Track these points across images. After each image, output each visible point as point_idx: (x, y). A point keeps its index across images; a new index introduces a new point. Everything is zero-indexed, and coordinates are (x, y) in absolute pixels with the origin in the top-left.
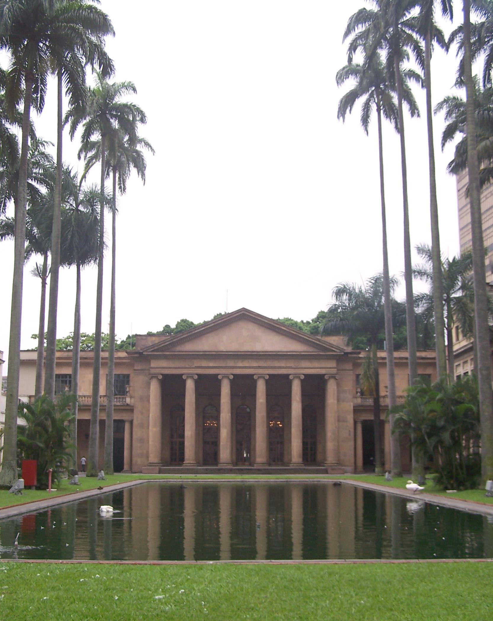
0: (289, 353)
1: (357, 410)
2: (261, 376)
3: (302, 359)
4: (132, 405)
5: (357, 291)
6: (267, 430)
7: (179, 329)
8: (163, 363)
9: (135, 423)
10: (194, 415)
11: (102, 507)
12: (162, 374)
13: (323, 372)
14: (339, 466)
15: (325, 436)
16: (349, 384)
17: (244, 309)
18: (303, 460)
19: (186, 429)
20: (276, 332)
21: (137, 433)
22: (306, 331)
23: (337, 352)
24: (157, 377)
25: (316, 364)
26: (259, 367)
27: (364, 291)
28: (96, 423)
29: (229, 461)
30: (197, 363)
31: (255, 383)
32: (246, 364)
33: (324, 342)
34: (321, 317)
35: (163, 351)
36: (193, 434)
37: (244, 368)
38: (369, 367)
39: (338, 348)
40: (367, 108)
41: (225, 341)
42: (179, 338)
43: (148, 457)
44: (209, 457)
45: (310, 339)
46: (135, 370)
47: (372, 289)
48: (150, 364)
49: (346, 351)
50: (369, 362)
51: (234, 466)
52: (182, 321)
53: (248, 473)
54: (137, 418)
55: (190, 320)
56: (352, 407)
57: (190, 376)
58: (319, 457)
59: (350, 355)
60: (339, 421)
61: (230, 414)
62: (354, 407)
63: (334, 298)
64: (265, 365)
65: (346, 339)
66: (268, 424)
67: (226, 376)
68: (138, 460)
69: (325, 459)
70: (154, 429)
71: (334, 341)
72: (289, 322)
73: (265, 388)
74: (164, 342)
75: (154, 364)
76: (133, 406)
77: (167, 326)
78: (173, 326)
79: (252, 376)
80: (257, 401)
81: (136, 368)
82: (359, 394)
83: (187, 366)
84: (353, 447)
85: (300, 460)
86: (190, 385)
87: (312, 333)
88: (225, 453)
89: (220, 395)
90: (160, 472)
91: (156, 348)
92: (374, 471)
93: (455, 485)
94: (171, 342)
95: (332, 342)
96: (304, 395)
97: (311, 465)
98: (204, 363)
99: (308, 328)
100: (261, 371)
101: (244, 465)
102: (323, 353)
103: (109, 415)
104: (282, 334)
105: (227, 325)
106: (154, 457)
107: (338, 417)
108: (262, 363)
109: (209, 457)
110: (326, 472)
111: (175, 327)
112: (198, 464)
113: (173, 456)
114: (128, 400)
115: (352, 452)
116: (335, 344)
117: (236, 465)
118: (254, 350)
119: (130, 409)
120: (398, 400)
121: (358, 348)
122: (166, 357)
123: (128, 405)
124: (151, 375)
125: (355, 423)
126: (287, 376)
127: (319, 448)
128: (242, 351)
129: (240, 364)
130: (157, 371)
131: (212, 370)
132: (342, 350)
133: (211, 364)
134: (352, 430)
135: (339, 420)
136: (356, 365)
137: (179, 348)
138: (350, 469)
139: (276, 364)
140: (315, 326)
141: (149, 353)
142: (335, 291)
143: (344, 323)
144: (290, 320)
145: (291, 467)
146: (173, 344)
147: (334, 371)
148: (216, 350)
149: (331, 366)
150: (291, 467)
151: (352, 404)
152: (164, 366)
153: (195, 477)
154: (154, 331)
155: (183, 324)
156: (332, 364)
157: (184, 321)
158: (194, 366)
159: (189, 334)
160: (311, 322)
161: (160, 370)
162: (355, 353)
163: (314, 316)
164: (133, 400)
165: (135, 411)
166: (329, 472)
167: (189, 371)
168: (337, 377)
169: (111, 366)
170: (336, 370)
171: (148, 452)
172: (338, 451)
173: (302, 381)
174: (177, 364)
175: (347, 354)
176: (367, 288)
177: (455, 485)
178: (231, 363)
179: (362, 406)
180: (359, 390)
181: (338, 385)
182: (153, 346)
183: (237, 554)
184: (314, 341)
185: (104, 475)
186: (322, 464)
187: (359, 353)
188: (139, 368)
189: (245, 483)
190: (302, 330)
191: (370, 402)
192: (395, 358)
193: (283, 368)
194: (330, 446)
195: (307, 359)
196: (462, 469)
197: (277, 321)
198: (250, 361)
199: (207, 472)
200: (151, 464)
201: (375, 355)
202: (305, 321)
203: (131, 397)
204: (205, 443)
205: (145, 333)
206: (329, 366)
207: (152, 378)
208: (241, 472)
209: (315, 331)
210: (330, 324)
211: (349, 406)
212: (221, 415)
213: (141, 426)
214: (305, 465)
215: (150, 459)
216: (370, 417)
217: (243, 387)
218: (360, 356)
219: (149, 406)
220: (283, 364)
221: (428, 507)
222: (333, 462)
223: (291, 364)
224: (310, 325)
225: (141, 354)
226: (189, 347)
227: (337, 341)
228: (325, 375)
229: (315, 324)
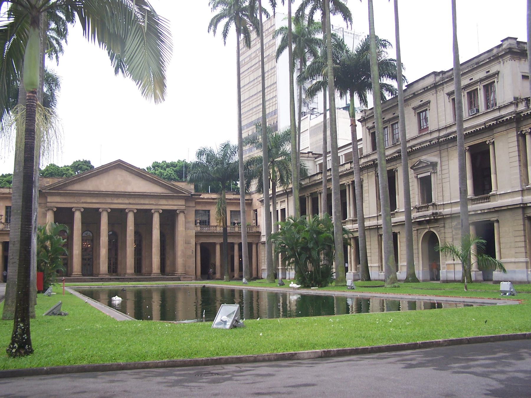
2: (131, 210)
8: (58, 199)
11: (114, 298)
13: (175, 208)
14: (185, 276)
17: (120, 161)
18: (161, 271)
20: (142, 178)
24: (52, 210)
25: (171, 202)
26: (130, 204)
30: (83, 199)
32: (120, 201)
33: (177, 187)
37: (119, 204)
39: (187, 191)
40: (227, 25)
41: (104, 184)
48: (46, 198)
53: (128, 281)
57: (78, 209)
60: (186, 243)
66: (82, 245)
67: (105, 210)
75: (49, 199)
83: (76, 202)
85: (159, 271)
86: (78, 216)
89: (160, 225)
93: (314, 284)
96: (84, 223)
98: (89, 200)
100: (131, 207)
102: (177, 194)
104: (147, 180)
108: (131, 201)
110: (179, 279)
118: (127, 191)
122: (60, 195)
130: (53, 205)
133: (94, 201)
135: (187, 243)
137: (70, 188)
138: (194, 277)
139: (142, 201)
145: (152, 276)
146: (65, 185)
147: (183, 208)
156: (182, 202)
162: (197, 195)
163: (150, 165)
166: (181, 279)
167: (78, 206)
172: (185, 266)
174: (68, 199)
177: (314, 284)
178: (109, 200)
181: (185, 218)
183: (271, 316)
192: (227, 199)
193: (147, 204)
194: (180, 261)
195: (163, 198)
196: (318, 273)
198: (123, 199)
206: (179, 204)
207: (49, 210)
211: (192, 233)
212: (101, 239)
217: (118, 218)
220: (147, 201)
221: (304, 297)
226: (77, 187)
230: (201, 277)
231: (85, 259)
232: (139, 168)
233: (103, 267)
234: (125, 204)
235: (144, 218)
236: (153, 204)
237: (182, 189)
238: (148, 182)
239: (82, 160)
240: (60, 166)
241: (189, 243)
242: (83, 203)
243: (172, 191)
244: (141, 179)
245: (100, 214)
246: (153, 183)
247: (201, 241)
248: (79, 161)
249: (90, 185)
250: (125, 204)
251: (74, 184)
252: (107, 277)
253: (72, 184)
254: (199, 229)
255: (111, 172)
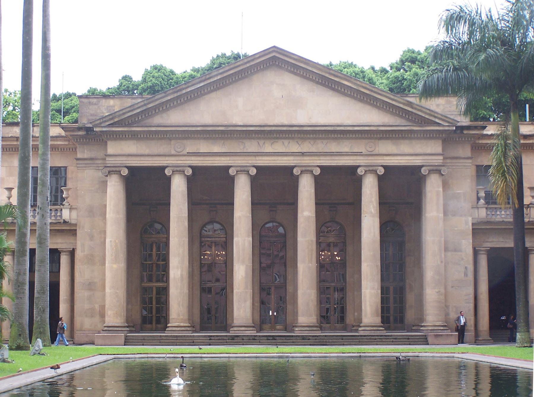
0: (356, 128)
1: (479, 230)
3: (380, 139)
4: (73, 222)
5: (484, 18)
6: (317, 267)
7: (150, 84)
9: (79, 254)
10: (186, 240)
12: (127, 167)
13: (416, 161)
15: (421, 277)
16: (465, 186)
17: (275, 49)
19: (171, 265)
20: (333, 89)
21: (83, 273)
22: (382, 87)
23: (439, 124)
25: (405, 147)
26: (303, 154)
27: (495, 17)
28: (26, 255)
29: (250, 322)
30: (191, 146)
31: (358, 182)
32: (279, 147)
34: (407, 60)
35: (130, 125)
36: (186, 274)
37: (276, 155)
38: (505, 155)
39: (445, 118)
42: (157, 102)
43: (102, 315)
44: (212, 316)
45: (394, 103)
46: (78, 159)
47: (511, 14)
49: (459, 124)
50: (506, 145)
51: (257, 332)
52: (155, 68)
54: (83, 246)
55: (169, 65)
56: (471, 224)
58: (410, 315)
59: (465, 132)
60: (446, 250)
61: (251, 239)
62: (473, 224)
63: (443, 30)
64: (313, 149)
65: (463, 103)
66: (318, 256)
68: (85, 322)
69: (421, 319)
70: (115, 266)
71: (438, 105)
72: (351, 70)
73: (313, 191)
74: (132, 108)
75: (112, 148)
76: (75, 225)
77: (127, 78)
78: (137, 77)
79: (290, 169)
80: (299, 215)
81: (79, 156)
82: (482, 201)
83: (173, 152)
84: (472, 296)
85: (378, 320)
86: (179, 187)
87: (391, 90)
88: (242, 307)
90: (127, 342)
91: (116, 120)
92: (512, 339)
94: (144, 108)
95: (433, 108)
96: (384, 203)
97: (395, 329)
99: (385, 81)
101: (273, 328)
103: (41, 242)
105: (246, 77)
106: (114, 316)
107: (446, 242)
108: (306, 147)
109: (212, 316)
110: (424, 341)
111: (140, 79)
112: (193, 328)
113: (148, 313)
114: (66, 214)
115: (472, 306)
116: (438, 110)
117: (261, 330)
118: (294, 122)
119: (69, 230)
120: (203, 231)
121: (480, 120)
122: (135, 136)
123: (65, 222)
124: (109, 169)
125: (476, 253)
126: (353, 169)
127: (410, 298)
128: (271, 124)
129: (268, 148)
130: (119, 161)
131: (218, 158)
132: (452, 122)
133: (216, 148)
134: (471, 267)
136: (479, 149)
137: (158, 120)
139: (333, 147)
140: (397, 77)
141: (104, 129)
142: (444, 18)
143: (461, 74)
144: (351, 65)
146: (148, 113)
147: (438, 160)
148: (226, 123)
149: (433, 152)
150: (362, 333)
151: (470, 220)
152: (130, 152)
153: (201, 351)
154: (103, 87)
155: (156, 75)
156: (436, 147)
157: (157, 68)
158: (185, 152)
159: (176, 95)
160: (388, 69)
161: (124, 158)
162: (476, 128)
163: (395, 57)
164: (74, 214)
165: (78, 232)
166: (430, 340)
167: (177, 161)
168: (444, 170)
169: (44, 154)
170: (441, 158)
171: (103, 307)
173: (381, 179)
175: (462, 128)
176: (502, 12)
178: (251, 146)
179: (488, 223)
180: (482, 194)
181: (445, 185)
182: (112, 115)
184: (401, 106)
185: (41, 347)
186: (418, 324)
187: (484, 128)
188: (86, 156)
189: (290, 359)
190: (374, 84)
191: (505, 215)
194: (431, 294)
197: (328, 68)
198: (286, 142)
199: (210, 342)
200: (110, 329)
201: (516, 130)
202: (377, 68)
203: (71, 209)
204: (205, 290)
205: (82, 91)
206: (429, 151)
208: (273, 341)
209: (399, 87)
210: (435, 76)
211: (465, 224)
212: (235, 239)
213: (90, 260)
214: (388, 329)
215: (107, 319)
216: (508, 242)
217: (275, 189)
218: (485, 132)
219: (105, 224)
220: (345, 147)
222: (438, 324)
223: (360, 147)
224: (388, 75)
225: (89, 130)
226: (176, 118)
227: (449, 108)
228: (422, 166)
229: (398, 74)
230: (491, 335)
231: (209, 290)
232: (318, 64)
233: (242, 307)
234: (293, 154)
235: (338, 189)
236: (360, 154)
237: (432, 113)
238: (348, 99)
239: (228, 54)
240: (179, 71)
241: (455, 250)
242: (190, 154)
243: (408, 120)
244: (331, 92)
245: (231, 180)
246: (361, 101)
247: (489, 245)
248: (224, 55)
249: (206, 113)
250: (293, 154)
251: (167, 110)
252: (248, 333)
253: (164, 111)
254: (483, 213)
255: (255, 77)
